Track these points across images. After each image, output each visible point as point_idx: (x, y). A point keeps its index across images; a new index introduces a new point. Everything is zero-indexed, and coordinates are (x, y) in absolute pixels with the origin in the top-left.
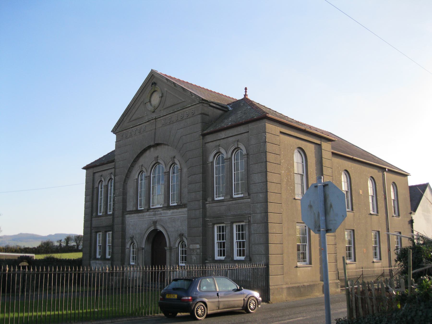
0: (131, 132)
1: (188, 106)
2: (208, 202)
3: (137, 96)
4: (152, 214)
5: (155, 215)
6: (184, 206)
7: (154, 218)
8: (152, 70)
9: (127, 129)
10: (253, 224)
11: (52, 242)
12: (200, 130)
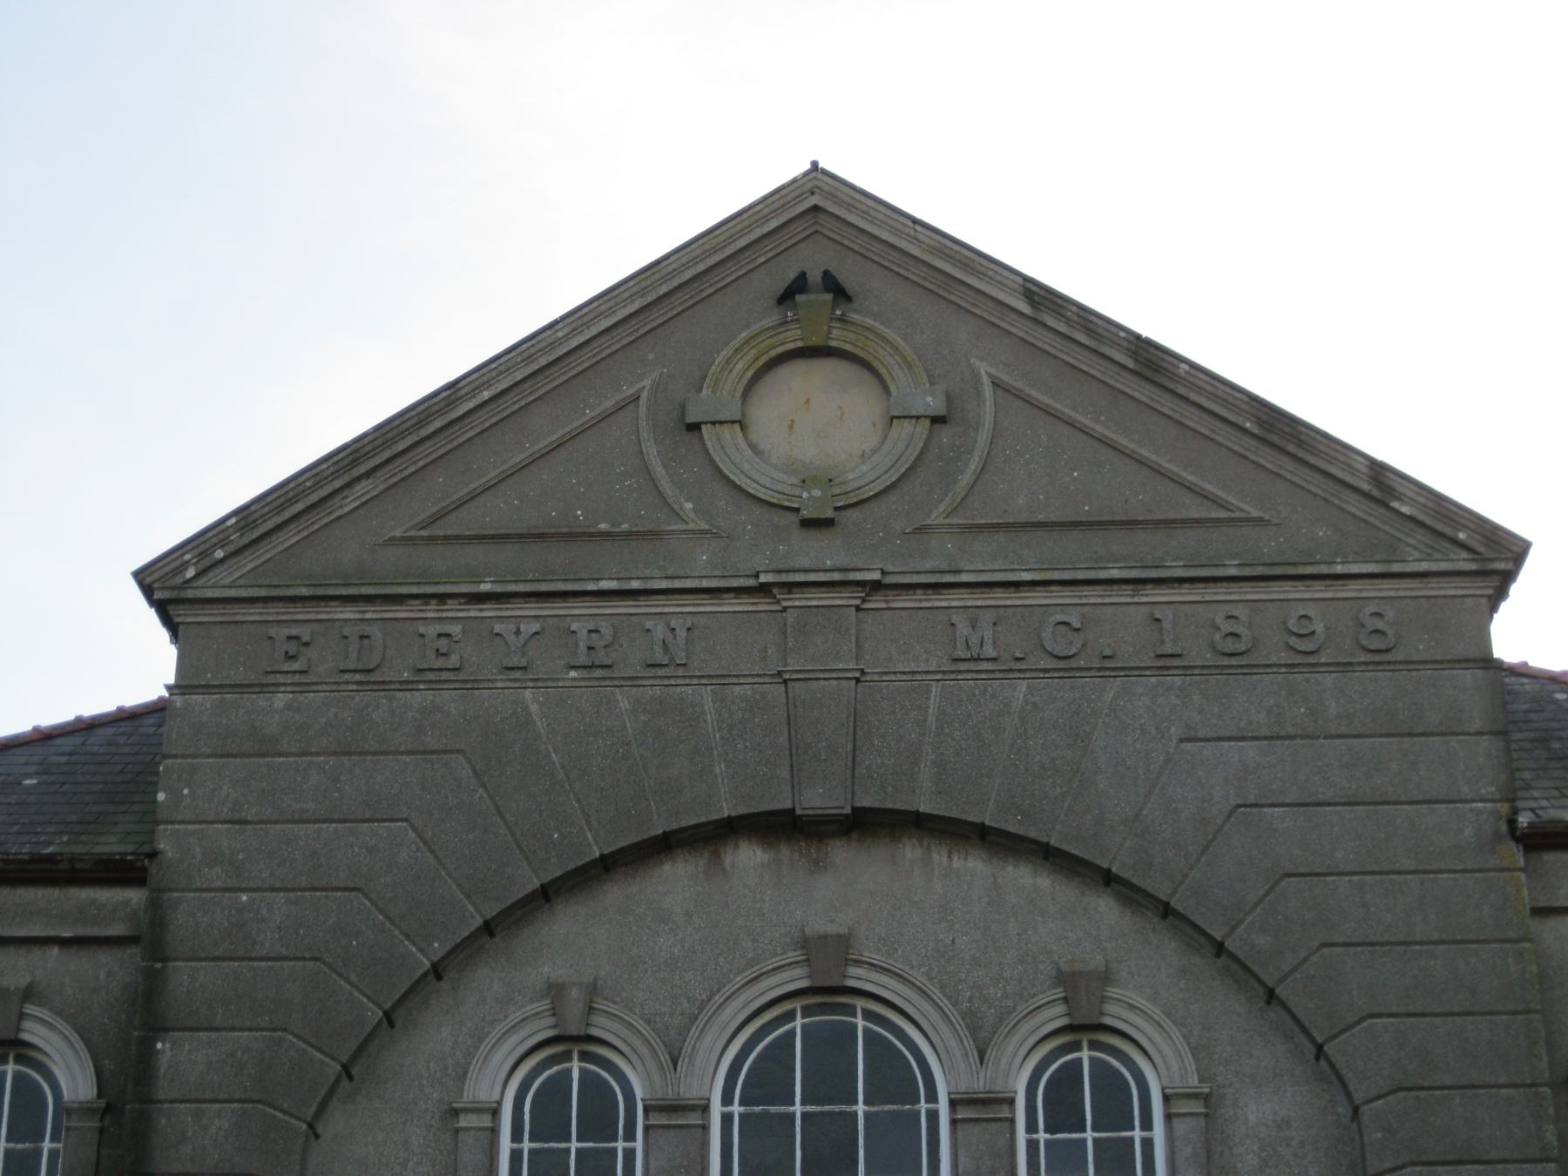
1: (1339, 569)
3: (575, 331)
8: (815, 165)
9: (399, 599)
12: (1489, 790)
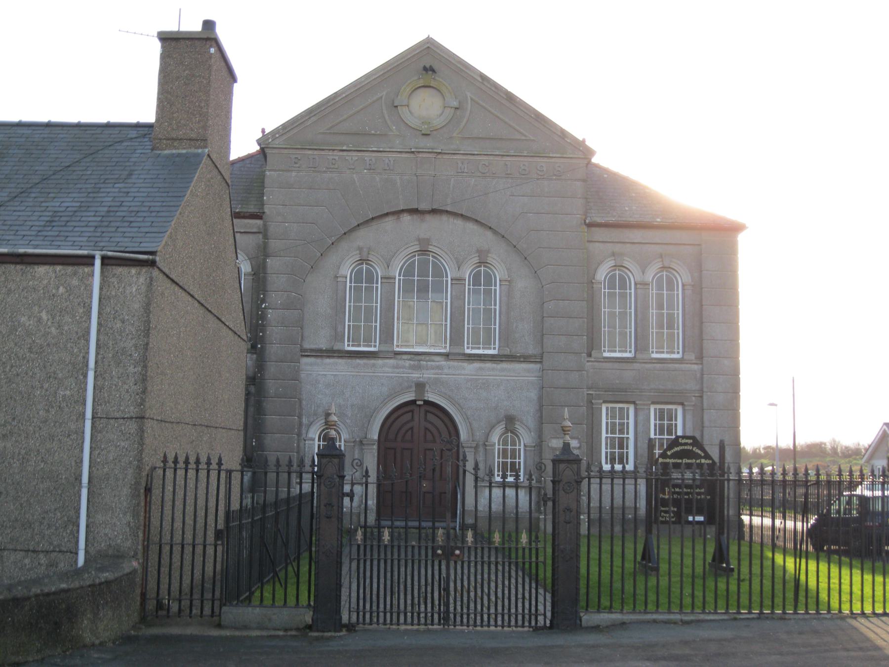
0: (337, 160)
1: (551, 155)
2: (593, 360)
4: (407, 365)
5: (418, 368)
6: (525, 358)
7: (416, 375)
9: (323, 150)
10: (709, 411)
11: (825, 444)
